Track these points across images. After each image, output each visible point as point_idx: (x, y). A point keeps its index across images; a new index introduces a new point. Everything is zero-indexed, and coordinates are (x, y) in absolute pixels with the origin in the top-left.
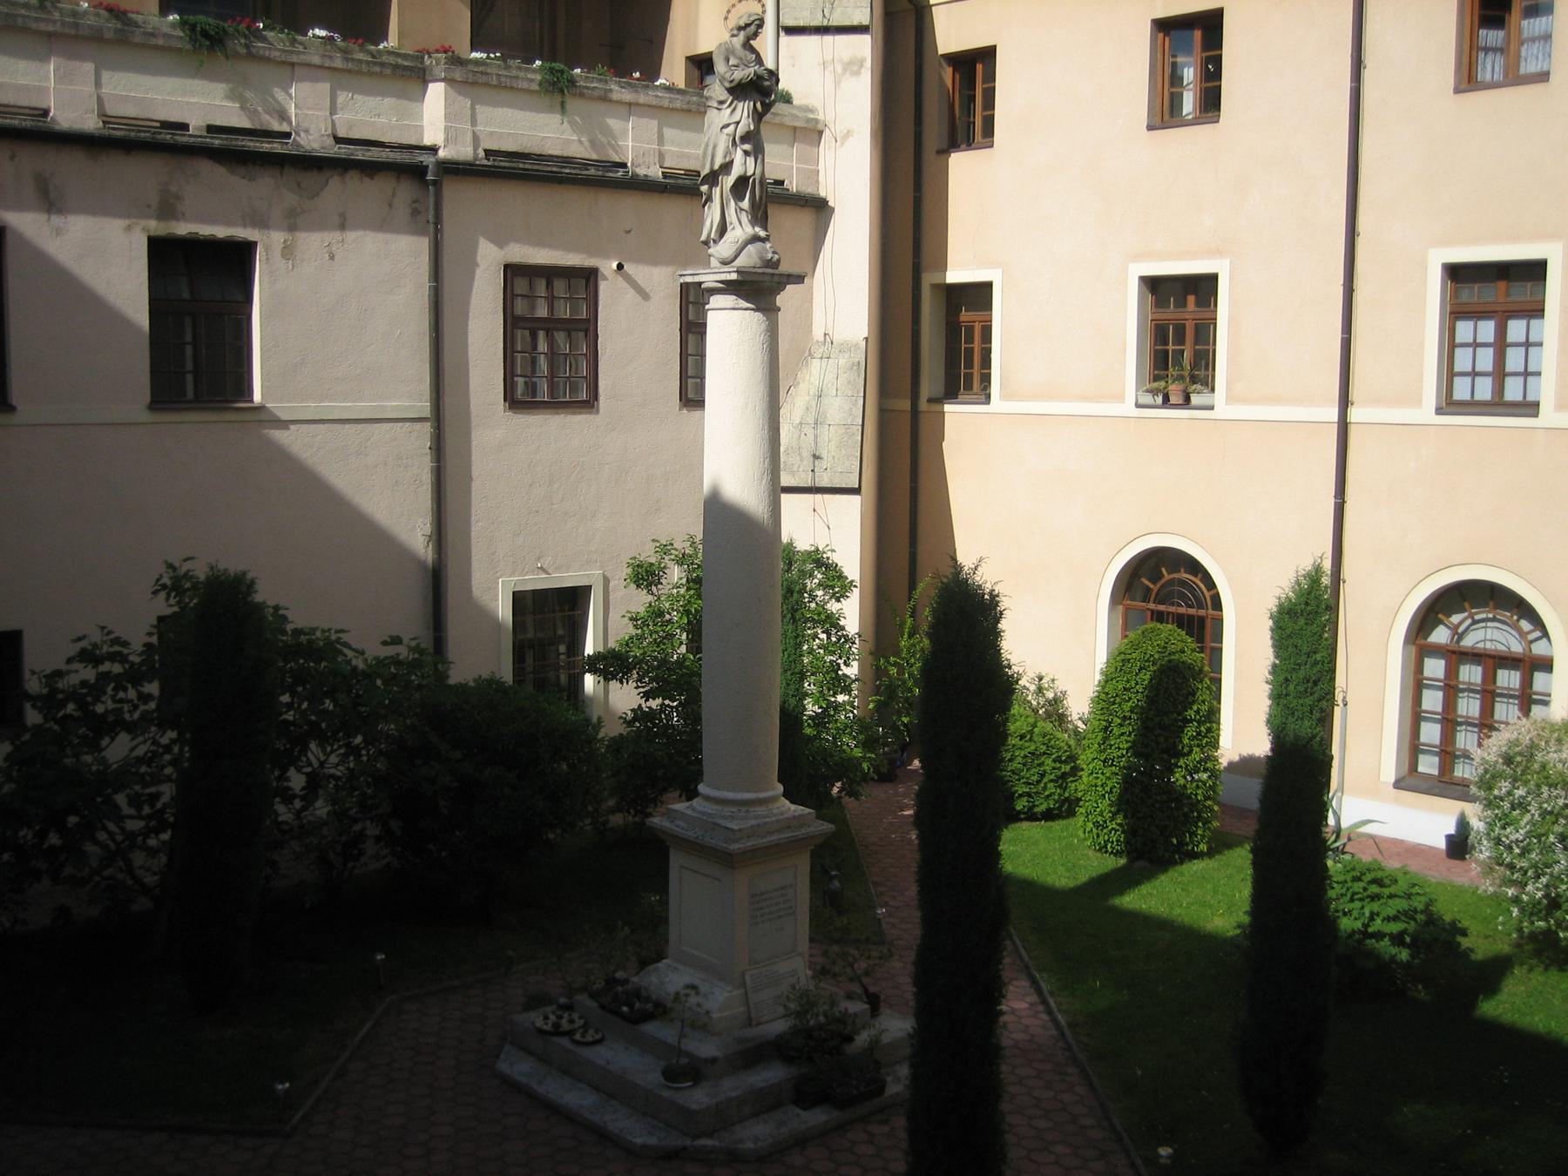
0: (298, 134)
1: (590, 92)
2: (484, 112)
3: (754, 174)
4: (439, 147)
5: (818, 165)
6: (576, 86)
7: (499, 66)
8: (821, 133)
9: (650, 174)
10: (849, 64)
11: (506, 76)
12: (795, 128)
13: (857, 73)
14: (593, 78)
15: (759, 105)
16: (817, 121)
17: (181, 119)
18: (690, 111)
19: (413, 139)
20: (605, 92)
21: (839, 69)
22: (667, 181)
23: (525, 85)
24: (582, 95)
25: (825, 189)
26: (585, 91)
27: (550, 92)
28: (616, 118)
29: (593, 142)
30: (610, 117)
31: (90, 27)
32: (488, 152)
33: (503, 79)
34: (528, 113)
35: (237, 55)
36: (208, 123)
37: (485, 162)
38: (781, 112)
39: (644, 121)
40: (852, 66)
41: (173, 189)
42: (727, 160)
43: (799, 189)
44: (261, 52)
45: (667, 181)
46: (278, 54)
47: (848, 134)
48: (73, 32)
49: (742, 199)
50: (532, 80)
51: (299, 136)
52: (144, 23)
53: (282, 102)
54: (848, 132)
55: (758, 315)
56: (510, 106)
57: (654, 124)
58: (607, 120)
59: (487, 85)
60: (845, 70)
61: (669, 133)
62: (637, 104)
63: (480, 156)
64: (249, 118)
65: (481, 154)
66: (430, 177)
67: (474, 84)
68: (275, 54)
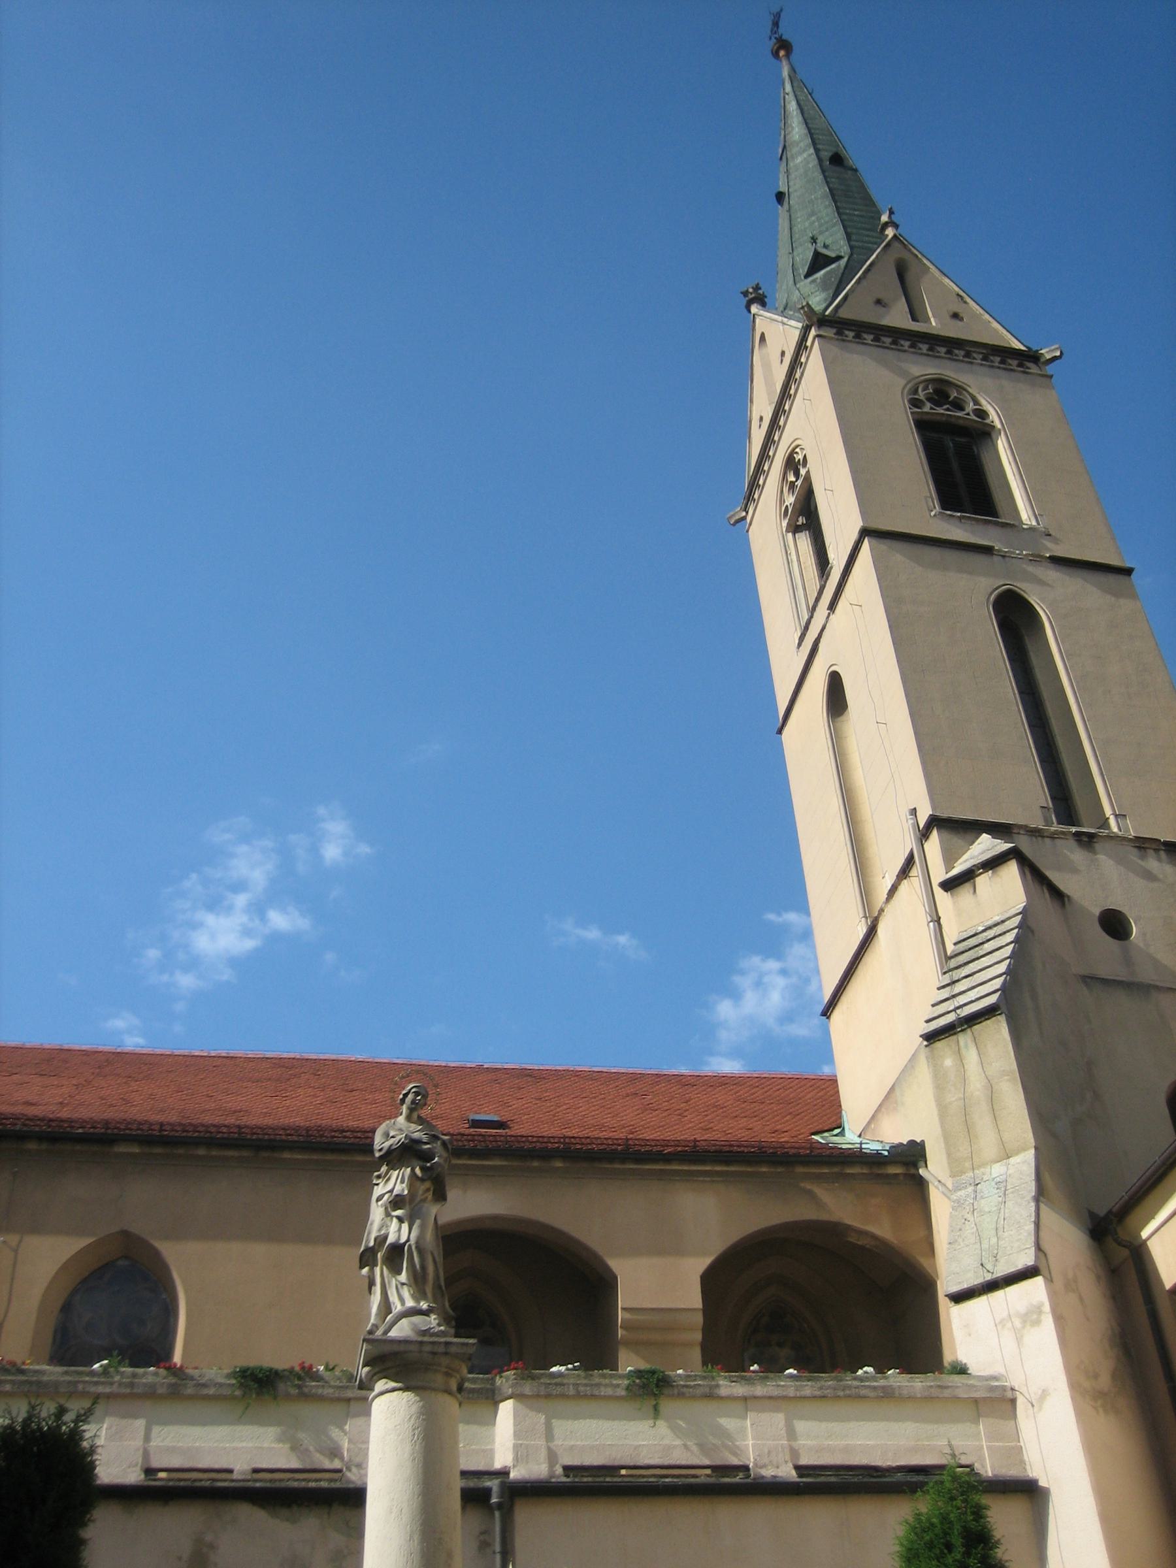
0: (349, 1469)
1: (691, 1390)
2: (561, 1427)
3: (408, 1240)
4: (510, 1467)
5: (1019, 1442)
6: (672, 1386)
7: (578, 1376)
8: (1013, 1401)
9: (780, 1474)
10: (1026, 1314)
11: (586, 1385)
12: (976, 1401)
13: (1037, 1323)
14: (696, 1376)
15: (418, 1171)
16: (1004, 1388)
17: (225, 1466)
18: (824, 1397)
19: (483, 1463)
20: (710, 1388)
21: (1018, 1323)
22: (804, 1480)
23: (610, 1391)
24: (681, 1395)
25: (1037, 1469)
26: (685, 1390)
27: (640, 1395)
28: (729, 1416)
29: (701, 1446)
30: (720, 1417)
31: (145, 1385)
32: (568, 1469)
33: (581, 1389)
34: (616, 1423)
35: (288, 1397)
36: (253, 1466)
37: (564, 1479)
38: (950, 1384)
39: (765, 1417)
40: (1031, 1317)
41: (209, 1537)
42: (382, 1232)
43: (996, 1473)
44: (314, 1391)
45: (804, 1480)
46: (331, 1391)
47: (1044, 1394)
48: (128, 1391)
49: (399, 1273)
50: (618, 1386)
51: (350, 1471)
52: (200, 1376)
53: (336, 1439)
54: (1044, 1391)
55: (408, 1396)
56: (592, 1417)
57: (779, 1419)
58: (718, 1419)
59: (563, 1396)
60: (1024, 1322)
61: (801, 1426)
62: (755, 1397)
63: (557, 1473)
64: (298, 1457)
65: (559, 1470)
66: (494, 1500)
67: (548, 1396)
68: (328, 1391)
